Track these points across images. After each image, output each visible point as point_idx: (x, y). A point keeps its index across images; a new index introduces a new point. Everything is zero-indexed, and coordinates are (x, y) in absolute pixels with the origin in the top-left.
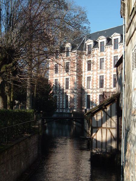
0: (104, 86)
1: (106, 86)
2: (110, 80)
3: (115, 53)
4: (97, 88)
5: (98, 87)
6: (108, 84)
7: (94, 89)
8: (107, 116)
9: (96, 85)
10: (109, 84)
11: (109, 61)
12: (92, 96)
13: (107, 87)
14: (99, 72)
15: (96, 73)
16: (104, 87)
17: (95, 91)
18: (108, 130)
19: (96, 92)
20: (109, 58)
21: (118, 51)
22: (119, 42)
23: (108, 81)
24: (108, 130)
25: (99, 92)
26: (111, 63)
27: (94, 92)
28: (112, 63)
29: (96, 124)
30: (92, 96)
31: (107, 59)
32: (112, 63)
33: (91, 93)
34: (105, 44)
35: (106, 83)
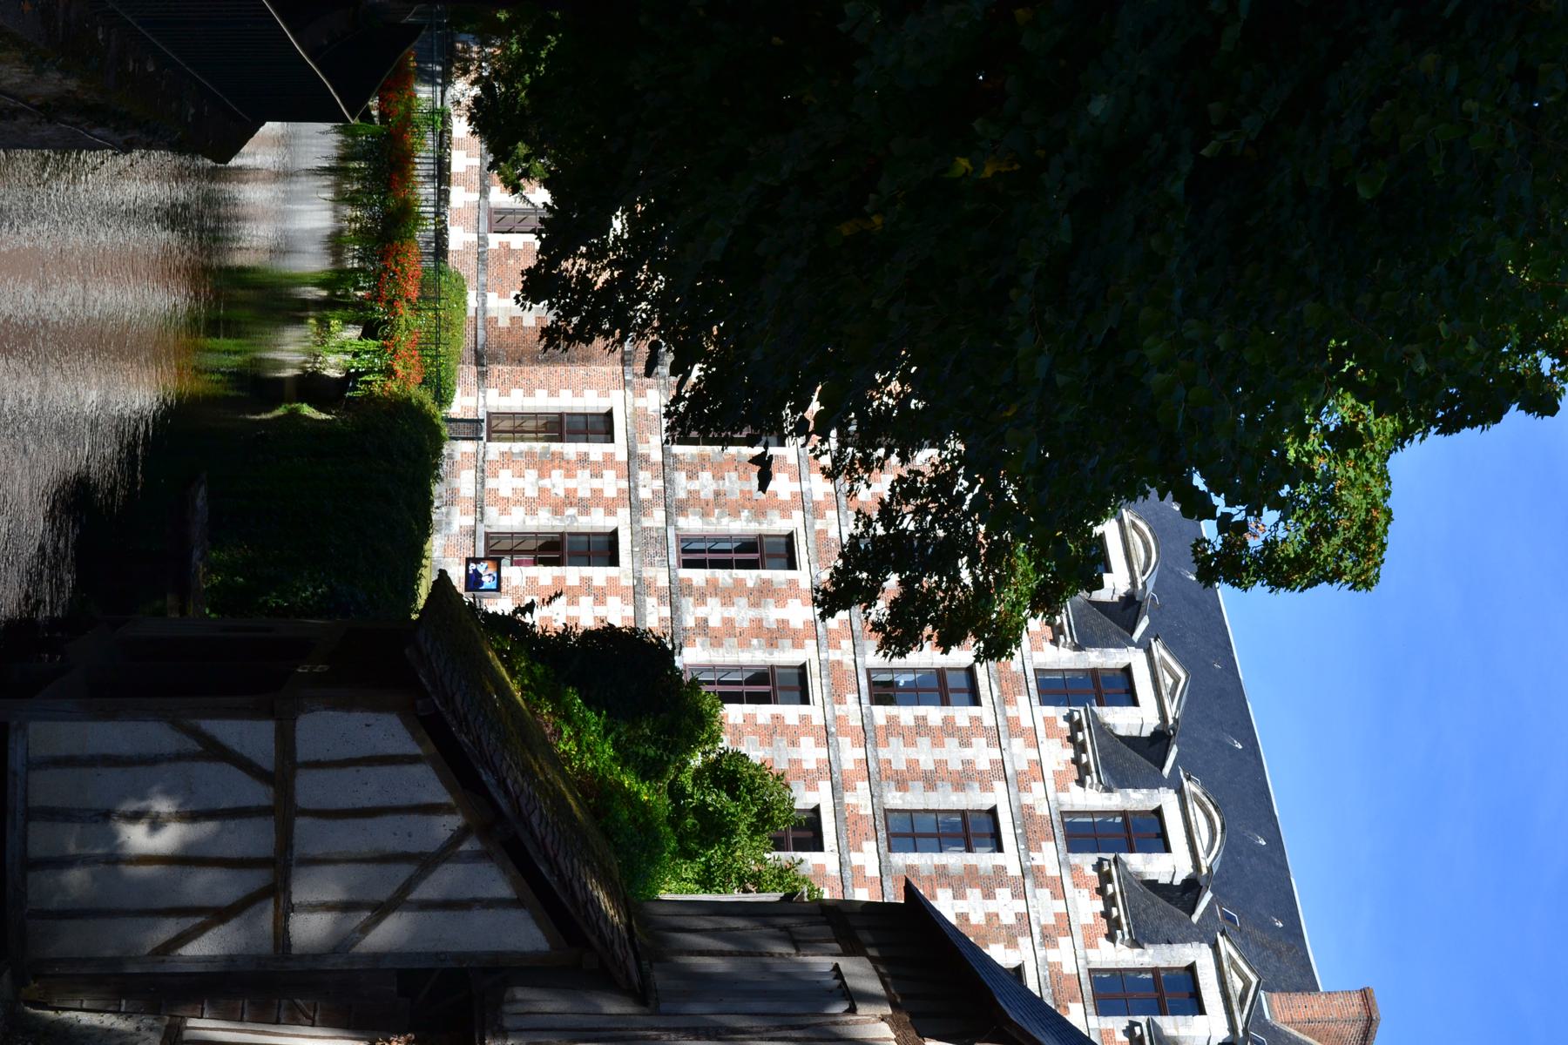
0: (698, 576)
1: (701, 598)
2: (758, 628)
3: (1025, 817)
4: (682, 508)
5: (692, 524)
6: (714, 611)
7: (675, 608)
8: (404, 871)
9: (707, 493)
10: (714, 622)
11: (953, 754)
12: (613, 587)
13: (687, 603)
14: (859, 799)
15: (818, 496)
16: (685, 573)
17: (648, 485)
18: (255, 880)
19: (644, 494)
20: (982, 755)
21: (1022, 700)
22: (1158, 1019)
23: (742, 613)
24: (255, 880)
25: (646, 522)
26: (921, 726)
27: (644, 476)
28: (921, 722)
29: (322, 756)
30: (613, 587)
31: (990, 883)
32: (921, 722)
33: (631, 454)
34: (1136, 862)
35: (727, 596)
